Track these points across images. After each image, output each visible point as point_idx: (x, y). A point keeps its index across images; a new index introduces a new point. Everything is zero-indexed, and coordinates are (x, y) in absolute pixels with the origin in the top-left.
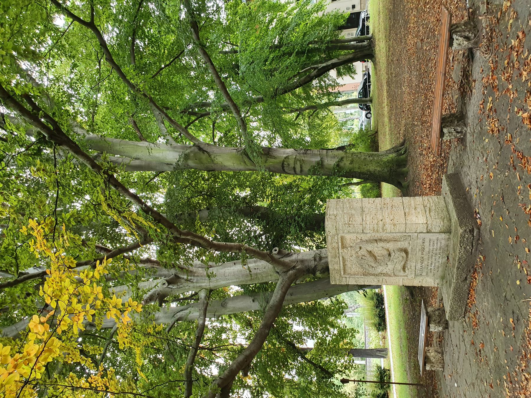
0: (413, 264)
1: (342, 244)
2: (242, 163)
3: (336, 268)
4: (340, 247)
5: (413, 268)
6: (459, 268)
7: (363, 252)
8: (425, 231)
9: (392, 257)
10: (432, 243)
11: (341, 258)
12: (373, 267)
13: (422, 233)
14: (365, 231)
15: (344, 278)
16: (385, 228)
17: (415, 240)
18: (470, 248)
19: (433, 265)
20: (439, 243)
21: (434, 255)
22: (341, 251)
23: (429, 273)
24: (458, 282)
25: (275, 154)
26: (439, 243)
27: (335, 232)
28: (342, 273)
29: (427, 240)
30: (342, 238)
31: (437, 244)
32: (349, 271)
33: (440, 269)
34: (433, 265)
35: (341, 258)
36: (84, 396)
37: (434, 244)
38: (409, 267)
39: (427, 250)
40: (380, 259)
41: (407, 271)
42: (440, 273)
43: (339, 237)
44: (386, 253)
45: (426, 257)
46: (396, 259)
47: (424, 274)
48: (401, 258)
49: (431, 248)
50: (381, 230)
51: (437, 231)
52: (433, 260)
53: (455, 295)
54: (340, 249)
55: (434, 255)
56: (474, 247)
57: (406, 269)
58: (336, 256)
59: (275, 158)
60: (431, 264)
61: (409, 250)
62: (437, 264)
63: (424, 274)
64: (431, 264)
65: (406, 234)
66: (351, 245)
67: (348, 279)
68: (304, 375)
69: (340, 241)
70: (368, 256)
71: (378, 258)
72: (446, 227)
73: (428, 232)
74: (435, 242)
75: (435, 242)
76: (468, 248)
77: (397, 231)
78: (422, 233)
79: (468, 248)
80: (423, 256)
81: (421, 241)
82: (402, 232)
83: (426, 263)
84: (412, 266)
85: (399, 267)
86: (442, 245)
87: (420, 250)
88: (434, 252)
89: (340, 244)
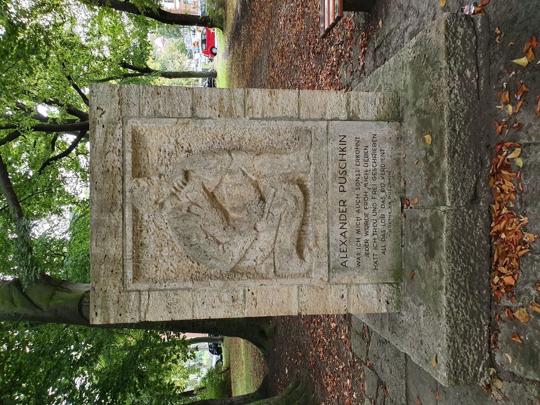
0: (322, 229)
1: (136, 163)
2: (7, 302)
3: (113, 251)
4: (129, 168)
5: (322, 243)
6: (455, 152)
7: (191, 193)
8: (343, 116)
9: (269, 201)
11: (128, 214)
12: (219, 243)
14: (199, 112)
15: (133, 296)
16: (248, 102)
17: (322, 145)
18: (473, 75)
20: (379, 154)
21: (370, 193)
22: (130, 183)
24: (459, 208)
25: (71, 287)
26: (379, 154)
27: (118, 113)
28: (129, 273)
29: (351, 144)
30: (137, 140)
32: (150, 271)
33: (389, 243)
34: (371, 230)
35: (128, 214)
38: (311, 244)
39: (351, 176)
40: (239, 220)
41: (307, 257)
42: (388, 260)
43: (128, 129)
44: (250, 194)
45: (351, 201)
46: (279, 205)
47: (351, 262)
48: (291, 203)
49: (362, 168)
50: (239, 109)
51: (370, 117)
52: (370, 211)
53: (456, 263)
54: (128, 177)
55: (370, 193)
56: (483, 72)
57: (306, 250)
58: (114, 204)
59: (69, 291)
60: (366, 223)
61: (309, 185)
62: (380, 227)
64: (366, 223)
65: (299, 124)
66: (162, 169)
67: (145, 296)
69: (128, 145)
70: (207, 204)
71: (233, 215)
72: (389, 107)
73: (350, 119)
74: (370, 150)
75: (370, 150)
76: (468, 73)
77: (279, 114)
78: (337, 119)
79: (468, 73)
80: (343, 196)
81: (336, 145)
82: (291, 119)
83: (352, 221)
84: (321, 234)
85: (287, 238)
87: (335, 175)
88: (370, 182)
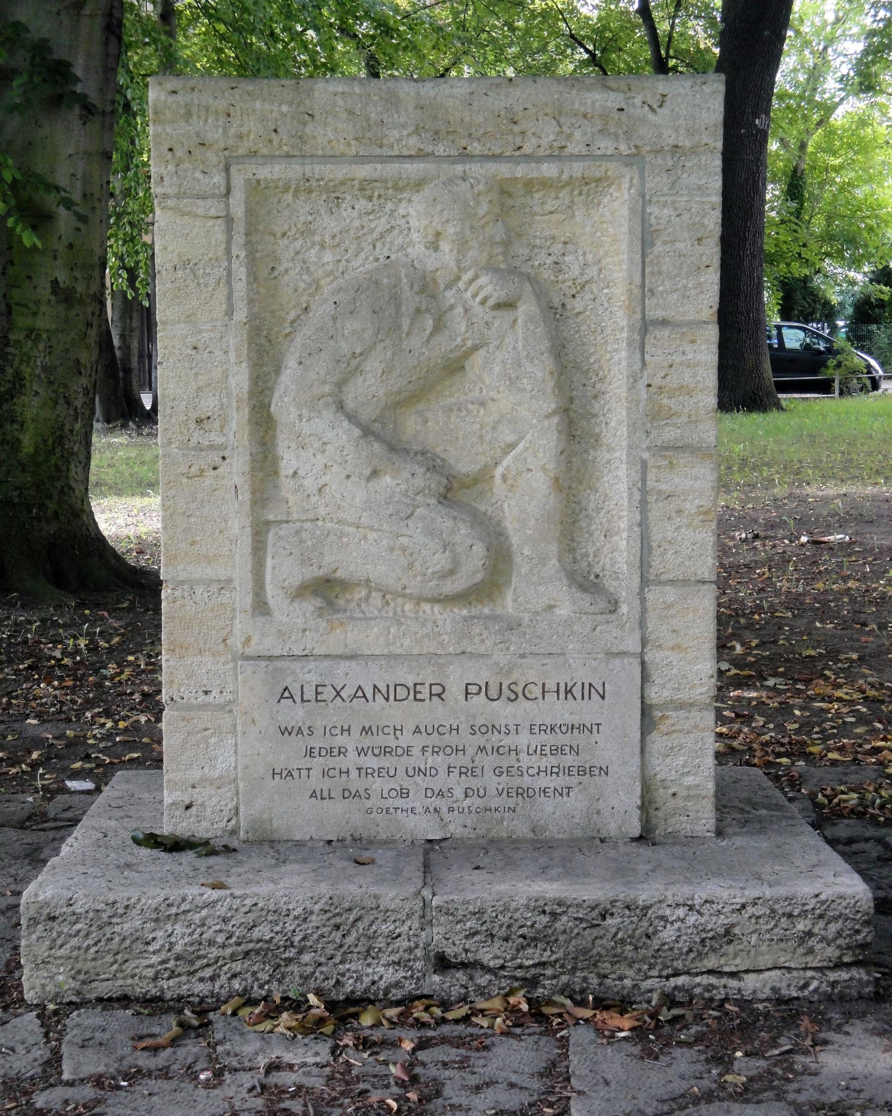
10: (560, 739)
13: (645, 678)
19: (370, 762)
20: (559, 782)
21: (461, 760)
23: (299, 743)
29: (586, 711)
31: (552, 772)
34: (370, 762)
35: (412, 169)
36: (887, 78)
37: (557, 750)
47: (296, 714)
49: (523, 740)
63: (296, 714)
68: (300, 137)
73: (646, 711)
75: (569, 760)
78: (645, 678)
86: (547, 805)
89: (548, 170)
